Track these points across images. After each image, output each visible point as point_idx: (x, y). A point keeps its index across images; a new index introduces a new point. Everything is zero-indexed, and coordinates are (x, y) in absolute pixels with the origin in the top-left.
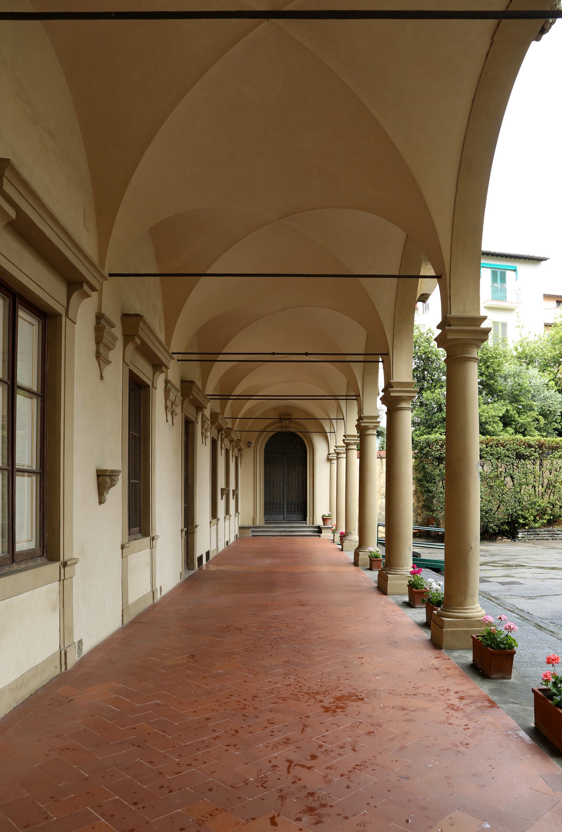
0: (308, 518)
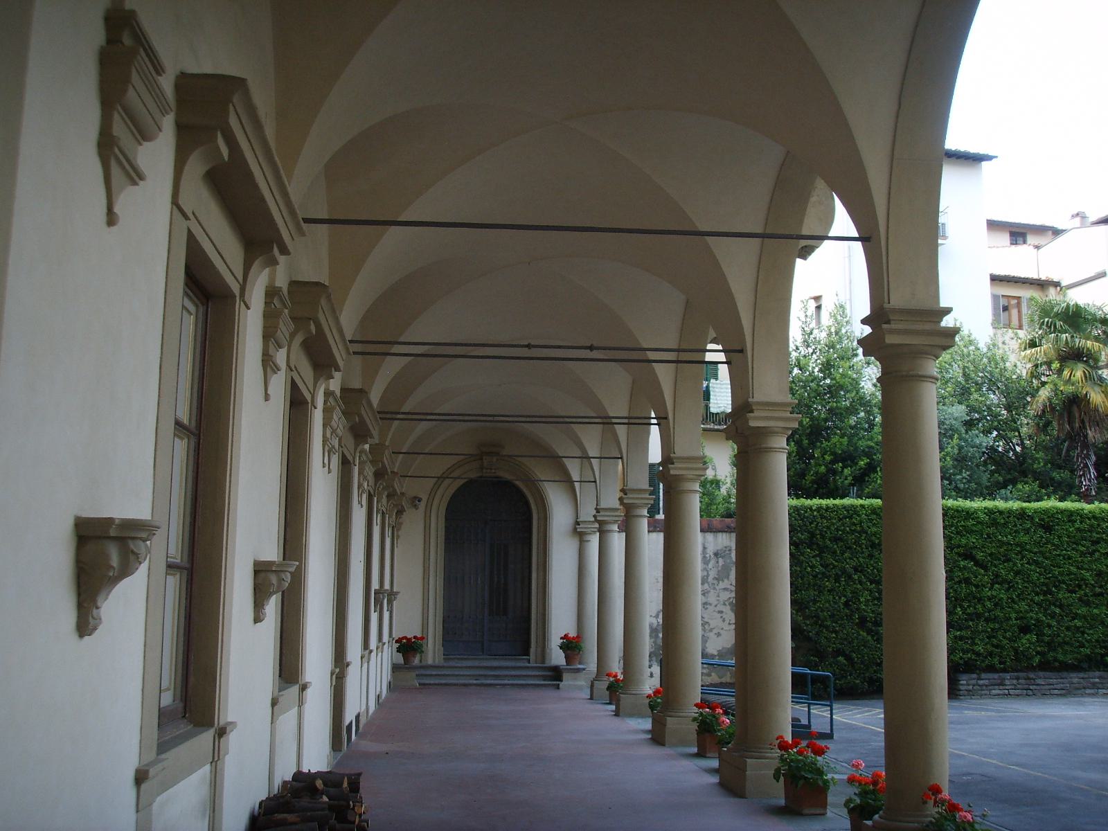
0: (532, 650)
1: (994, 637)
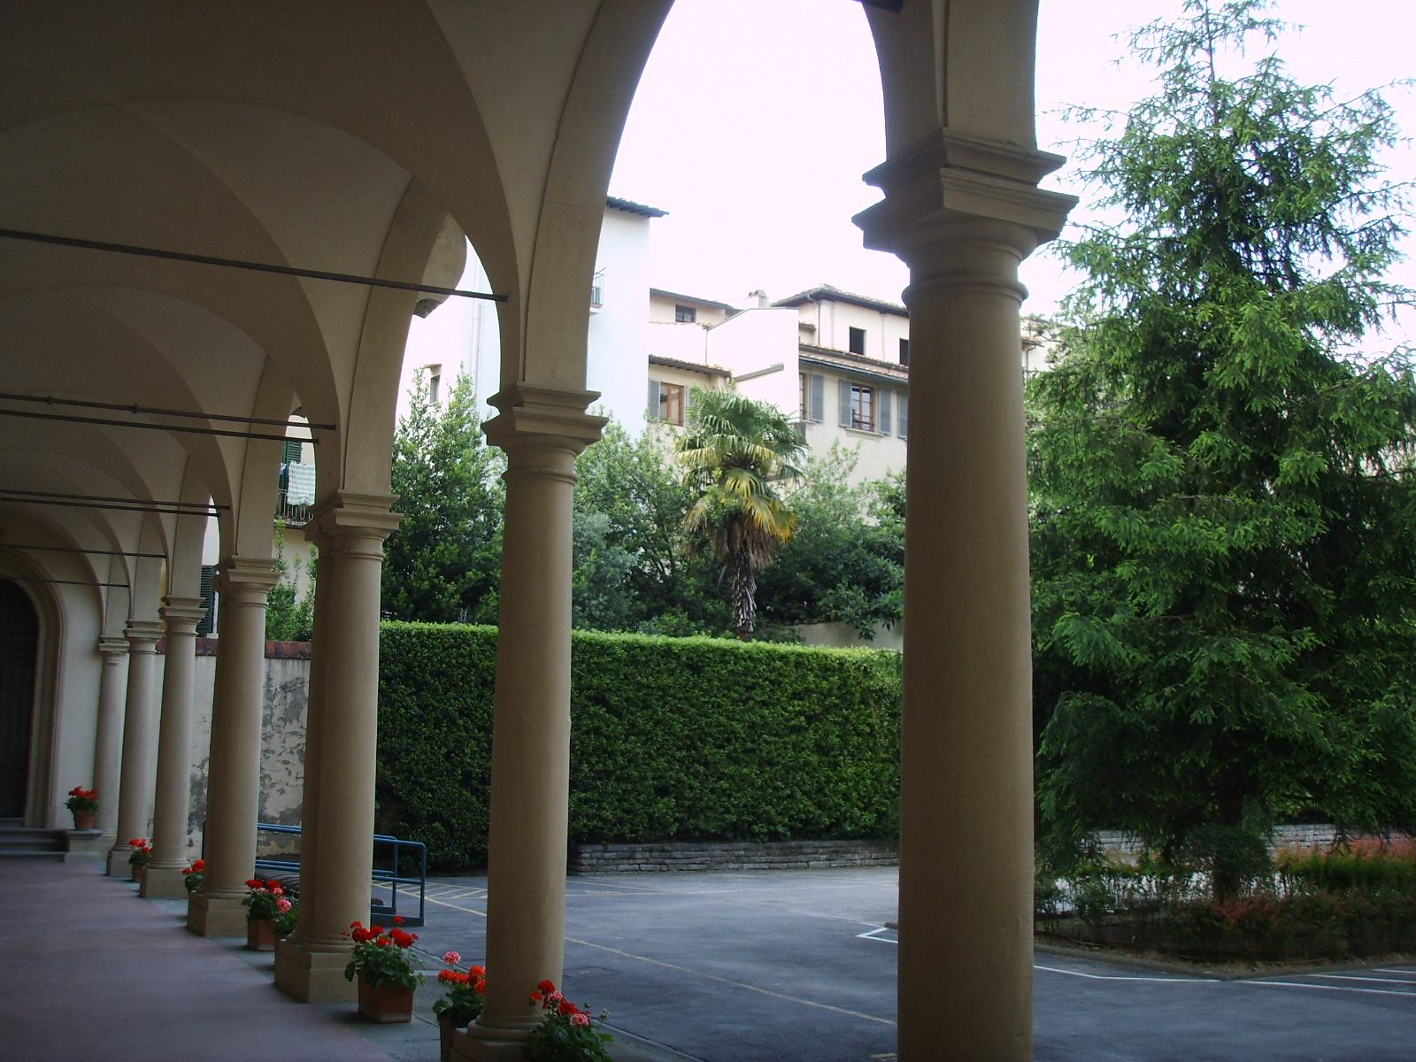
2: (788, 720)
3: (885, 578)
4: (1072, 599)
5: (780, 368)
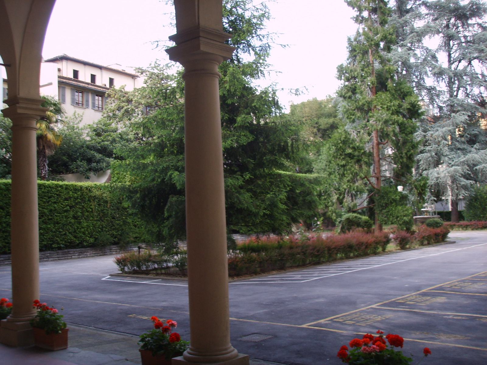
1: (6, 239)
2: (63, 208)
3: (93, 158)
4: (172, 164)
5: (50, 84)
